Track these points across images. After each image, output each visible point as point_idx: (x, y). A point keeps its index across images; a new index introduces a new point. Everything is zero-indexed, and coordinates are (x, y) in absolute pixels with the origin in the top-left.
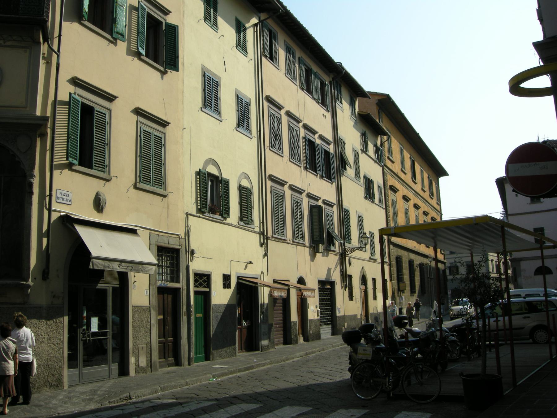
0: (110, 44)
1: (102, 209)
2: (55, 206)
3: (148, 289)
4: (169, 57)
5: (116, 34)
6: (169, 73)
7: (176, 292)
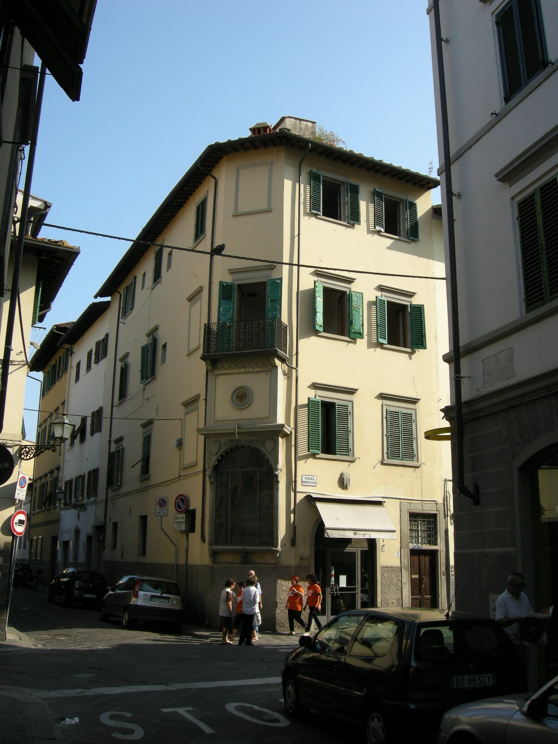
0: (349, 344)
1: (346, 486)
2: (300, 488)
3: (400, 551)
4: (415, 338)
5: (353, 334)
6: (417, 351)
7: (434, 554)
